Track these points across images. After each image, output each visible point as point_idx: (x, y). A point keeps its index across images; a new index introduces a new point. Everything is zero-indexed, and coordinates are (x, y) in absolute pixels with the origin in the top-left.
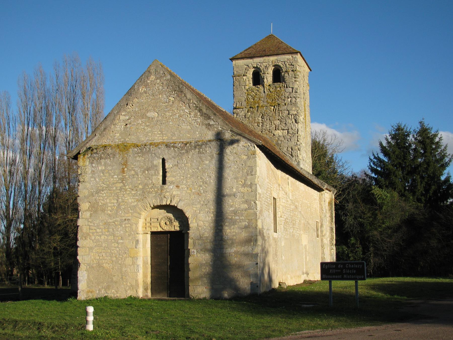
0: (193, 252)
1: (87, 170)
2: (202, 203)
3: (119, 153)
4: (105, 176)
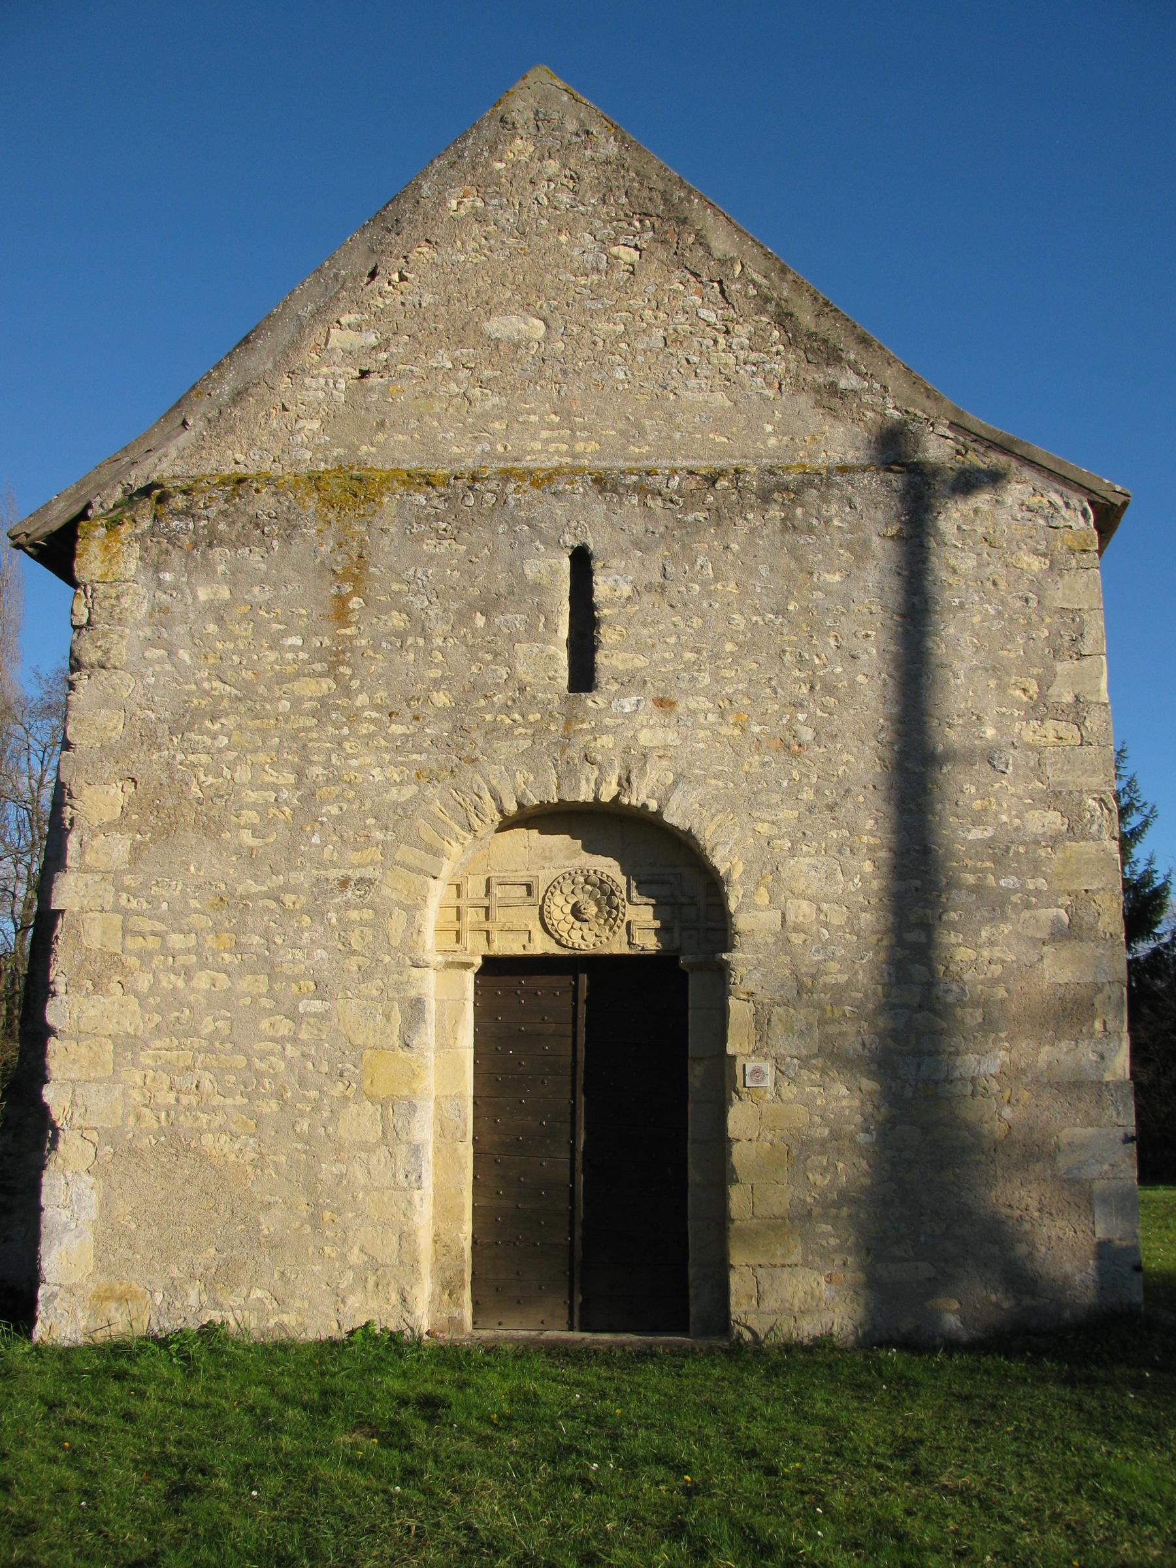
0: (757, 1072)
1: (126, 602)
2: (807, 795)
3: (319, 516)
4: (234, 638)
